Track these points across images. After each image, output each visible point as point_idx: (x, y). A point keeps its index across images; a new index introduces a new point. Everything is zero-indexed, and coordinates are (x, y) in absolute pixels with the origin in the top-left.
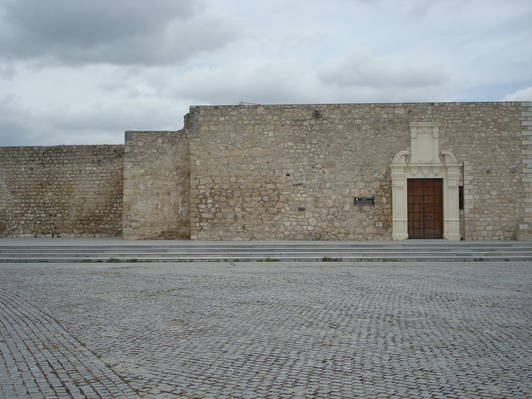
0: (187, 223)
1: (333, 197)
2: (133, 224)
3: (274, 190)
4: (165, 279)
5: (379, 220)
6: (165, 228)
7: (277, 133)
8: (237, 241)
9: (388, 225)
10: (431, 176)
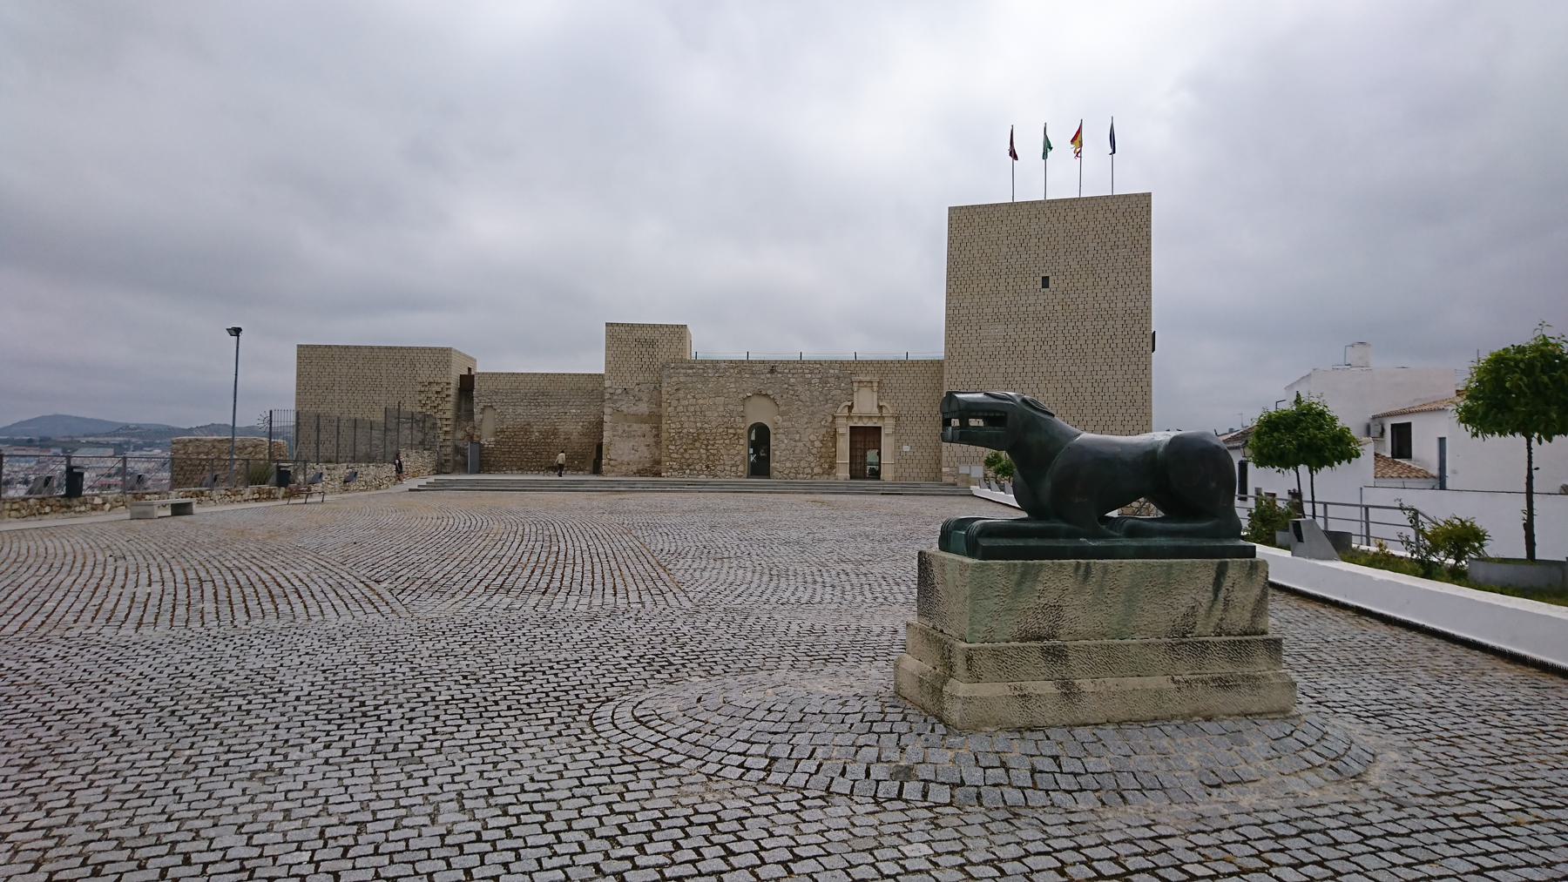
0: (658, 462)
8: (702, 478)
9: (832, 466)
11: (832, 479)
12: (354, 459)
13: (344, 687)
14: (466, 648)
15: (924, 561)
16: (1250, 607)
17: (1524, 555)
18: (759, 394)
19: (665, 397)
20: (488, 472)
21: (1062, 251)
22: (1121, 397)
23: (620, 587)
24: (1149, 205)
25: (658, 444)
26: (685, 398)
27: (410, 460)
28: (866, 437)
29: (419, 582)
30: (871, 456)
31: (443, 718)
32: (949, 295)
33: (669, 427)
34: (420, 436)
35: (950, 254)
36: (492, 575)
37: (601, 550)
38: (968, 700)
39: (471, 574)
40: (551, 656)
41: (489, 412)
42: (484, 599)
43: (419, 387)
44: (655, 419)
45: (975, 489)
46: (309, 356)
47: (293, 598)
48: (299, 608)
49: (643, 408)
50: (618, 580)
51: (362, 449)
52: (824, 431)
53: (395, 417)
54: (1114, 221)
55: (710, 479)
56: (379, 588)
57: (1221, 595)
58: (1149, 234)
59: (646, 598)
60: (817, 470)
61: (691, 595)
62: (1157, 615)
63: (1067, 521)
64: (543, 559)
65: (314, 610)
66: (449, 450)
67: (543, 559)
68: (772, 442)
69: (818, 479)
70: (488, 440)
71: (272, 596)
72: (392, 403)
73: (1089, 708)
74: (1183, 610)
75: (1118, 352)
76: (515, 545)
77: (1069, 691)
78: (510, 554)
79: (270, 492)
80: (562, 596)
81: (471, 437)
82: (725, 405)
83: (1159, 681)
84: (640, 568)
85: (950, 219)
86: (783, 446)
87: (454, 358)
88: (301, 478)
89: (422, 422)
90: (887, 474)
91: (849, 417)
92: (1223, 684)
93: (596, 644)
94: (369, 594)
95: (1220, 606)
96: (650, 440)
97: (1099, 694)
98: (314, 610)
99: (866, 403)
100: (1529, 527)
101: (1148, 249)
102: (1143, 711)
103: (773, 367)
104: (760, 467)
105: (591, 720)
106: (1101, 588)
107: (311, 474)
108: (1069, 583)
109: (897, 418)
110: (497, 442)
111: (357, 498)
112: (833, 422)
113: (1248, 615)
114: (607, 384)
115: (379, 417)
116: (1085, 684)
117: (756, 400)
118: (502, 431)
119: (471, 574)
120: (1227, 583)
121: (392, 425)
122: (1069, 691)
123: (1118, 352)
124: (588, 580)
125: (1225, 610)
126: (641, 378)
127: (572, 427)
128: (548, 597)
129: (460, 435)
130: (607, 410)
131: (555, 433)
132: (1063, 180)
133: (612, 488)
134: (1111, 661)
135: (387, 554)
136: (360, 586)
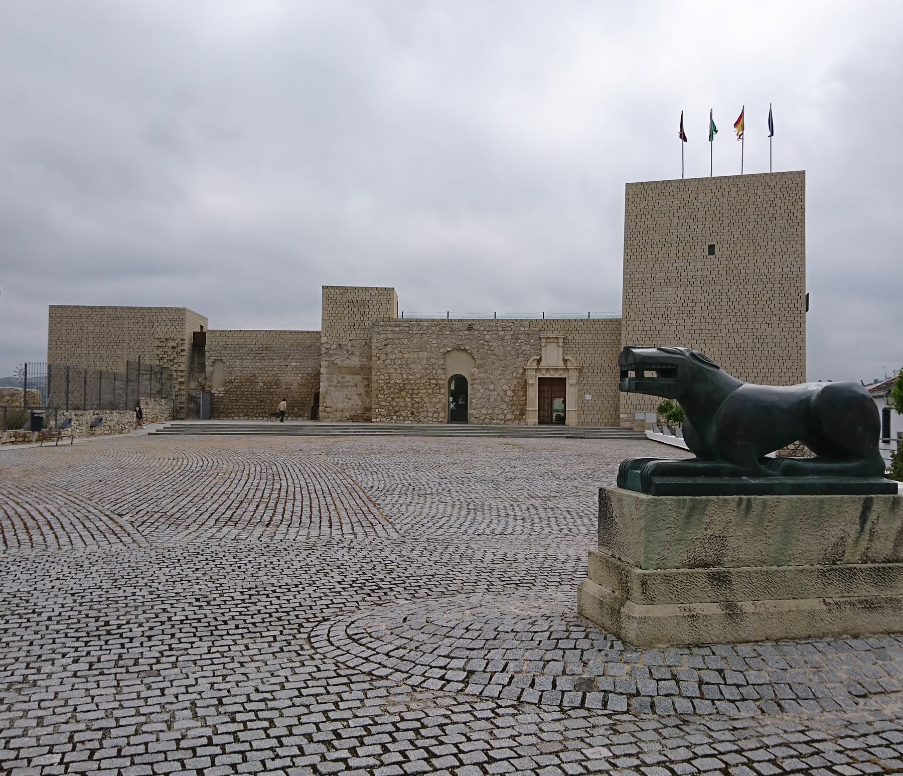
0: (369, 409)
1: (482, 391)
2: (328, 410)
3: (436, 385)
4: (568, 511)
5: (517, 409)
6: (353, 413)
7: (439, 341)
8: (408, 423)
9: (523, 413)
10: (556, 376)
11: (522, 424)
12: (100, 407)
14: (199, 574)
15: (604, 497)
18: (458, 349)
19: (374, 351)
20: (218, 418)
21: (726, 222)
22: (779, 351)
23: (335, 520)
24: (803, 182)
25: (368, 393)
26: (393, 352)
27: (149, 407)
28: (552, 387)
29: (157, 516)
30: (557, 403)
31: (178, 635)
33: (379, 379)
34: (158, 386)
36: (221, 510)
38: (643, 620)
39: (203, 509)
40: (273, 581)
41: (219, 365)
42: (214, 530)
43: (157, 343)
44: (366, 371)
45: (649, 433)
46: (58, 314)
47: (46, 529)
48: (51, 538)
49: (355, 361)
51: (107, 397)
52: (515, 382)
53: (136, 370)
54: (772, 196)
55: (415, 424)
56: (122, 521)
59: (358, 529)
60: (509, 416)
61: (398, 527)
62: (811, 545)
63: (730, 461)
64: (266, 495)
65: (64, 540)
66: (183, 398)
67: (266, 495)
69: (510, 424)
70: (218, 389)
71: (26, 528)
72: (133, 357)
73: (750, 628)
74: (833, 540)
75: (776, 311)
76: (242, 483)
77: (732, 612)
79: (25, 436)
80: (283, 528)
81: (203, 387)
83: (811, 603)
84: (352, 503)
85: (627, 194)
86: (479, 395)
87: (188, 317)
88: (52, 423)
89: (160, 373)
93: (314, 570)
94: (113, 526)
95: (866, 536)
96: (362, 390)
97: (759, 614)
98: (64, 540)
99: (552, 358)
101: (803, 220)
102: (798, 629)
103: (470, 325)
105: (309, 637)
107: (61, 419)
108: (732, 516)
109: (580, 370)
110: (226, 392)
111: (103, 441)
112: (523, 374)
113: (890, 545)
115: (122, 369)
116: (747, 606)
117: (455, 354)
118: (231, 382)
119: (203, 509)
121: (133, 377)
122: (732, 612)
123: (776, 311)
124: (306, 514)
125: (871, 540)
126: (353, 335)
127: (292, 378)
128: (271, 529)
129: (193, 385)
131: (277, 383)
132: (727, 160)
133: (327, 433)
134: (769, 585)
135: (128, 491)
136: (105, 519)
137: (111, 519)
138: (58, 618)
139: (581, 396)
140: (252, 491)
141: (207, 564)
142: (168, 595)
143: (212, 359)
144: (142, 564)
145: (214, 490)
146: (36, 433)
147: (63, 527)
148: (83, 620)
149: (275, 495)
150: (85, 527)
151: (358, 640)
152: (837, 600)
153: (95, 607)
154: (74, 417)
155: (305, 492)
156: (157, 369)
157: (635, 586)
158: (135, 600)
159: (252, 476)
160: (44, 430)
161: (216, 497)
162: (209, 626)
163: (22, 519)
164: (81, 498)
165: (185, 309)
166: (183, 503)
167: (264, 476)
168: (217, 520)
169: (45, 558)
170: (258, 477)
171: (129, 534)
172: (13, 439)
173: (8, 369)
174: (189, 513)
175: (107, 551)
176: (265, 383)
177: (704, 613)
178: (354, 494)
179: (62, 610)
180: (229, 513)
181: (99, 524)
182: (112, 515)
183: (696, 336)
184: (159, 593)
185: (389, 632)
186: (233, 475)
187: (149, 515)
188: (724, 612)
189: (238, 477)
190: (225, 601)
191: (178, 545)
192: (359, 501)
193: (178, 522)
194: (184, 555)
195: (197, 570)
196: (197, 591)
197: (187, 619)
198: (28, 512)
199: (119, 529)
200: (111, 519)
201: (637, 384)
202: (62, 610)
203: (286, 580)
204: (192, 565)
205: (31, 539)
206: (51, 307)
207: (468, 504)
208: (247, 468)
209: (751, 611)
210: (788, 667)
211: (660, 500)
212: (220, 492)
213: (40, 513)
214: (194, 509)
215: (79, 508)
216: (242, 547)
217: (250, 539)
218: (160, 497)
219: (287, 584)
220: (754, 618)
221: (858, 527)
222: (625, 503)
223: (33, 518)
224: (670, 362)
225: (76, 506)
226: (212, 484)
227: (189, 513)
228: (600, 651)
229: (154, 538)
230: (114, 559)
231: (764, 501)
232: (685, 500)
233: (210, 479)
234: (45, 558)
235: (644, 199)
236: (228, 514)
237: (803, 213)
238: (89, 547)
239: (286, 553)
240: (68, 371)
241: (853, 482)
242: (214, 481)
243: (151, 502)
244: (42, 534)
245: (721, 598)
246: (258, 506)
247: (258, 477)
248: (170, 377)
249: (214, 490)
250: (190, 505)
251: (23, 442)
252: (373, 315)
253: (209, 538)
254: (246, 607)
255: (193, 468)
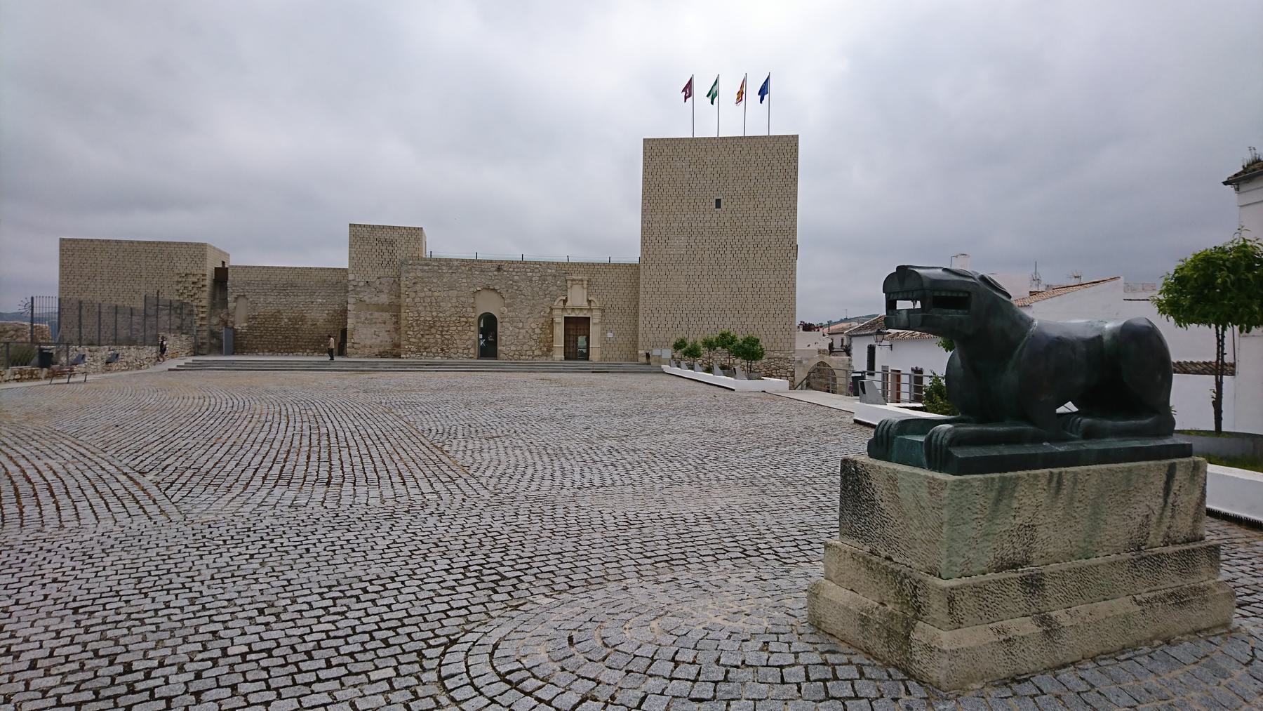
0: (398, 346)
6: (382, 349)
8: (438, 359)
9: (550, 349)
11: (550, 360)
12: (116, 342)
13: (103, 638)
14: (255, 564)
15: (849, 471)
16: (1192, 511)
17: (1213, 428)
18: (488, 289)
19: (403, 289)
20: (242, 353)
21: (731, 178)
22: (773, 295)
23: (406, 474)
24: (797, 145)
25: (397, 330)
26: (422, 291)
27: (172, 342)
28: (578, 326)
29: (188, 473)
30: (581, 340)
31: (243, 688)
32: (644, 211)
33: (407, 316)
34: (178, 321)
35: (644, 178)
36: (267, 463)
37: (370, 431)
38: (955, 654)
39: (245, 462)
40: (358, 571)
41: (242, 301)
42: (264, 493)
43: (176, 278)
44: (395, 309)
45: (666, 368)
46: (69, 248)
47: (44, 496)
48: (49, 510)
49: (384, 299)
50: (401, 465)
51: (123, 333)
52: (542, 320)
53: (154, 305)
54: (770, 156)
55: (445, 360)
56: (146, 481)
57: (1170, 501)
58: (796, 168)
59: (438, 486)
60: (537, 353)
61: (483, 481)
62: (1118, 527)
63: (1032, 423)
64: (315, 442)
65: (67, 513)
66: (205, 334)
67: (315, 442)
68: (499, 329)
69: (537, 360)
70: (241, 325)
71: (17, 495)
72: (152, 292)
73: (1070, 646)
74: (1139, 519)
75: (772, 260)
76: (283, 426)
77: (1050, 628)
78: (280, 436)
79: (32, 373)
80: (348, 485)
81: (225, 323)
82: (457, 297)
83: (1122, 605)
84: (417, 450)
85: (645, 148)
86: (508, 333)
87: (209, 252)
88: (64, 359)
89: (180, 309)
90: (595, 355)
91: (564, 309)
92: (1178, 599)
93: (406, 551)
94: (133, 489)
95: (1168, 513)
96: (390, 327)
97: (1077, 626)
98: (67, 513)
99: (577, 298)
100: (1217, 404)
101: (796, 180)
102: (1114, 642)
103: (499, 266)
104: (489, 350)
105: (441, 679)
106: (1072, 499)
107: (73, 356)
108: (1043, 497)
109: (603, 311)
110: (249, 328)
111: (118, 377)
112: (550, 313)
113: (1190, 521)
114: (351, 277)
115: (139, 305)
116: (1059, 614)
117: (485, 293)
118: (254, 318)
119: (245, 462)
120: (1175, 488)
121: (151, 312)
122: (1050, 628)
123: (772, 260)
124: (369, 468)
125: (1173, 517)
126: (381, 273)
127: (318, 314)
128: (333, 489)
129: (215, 321)
130: (351, 300)
131: (303, 319)
132: (729, 121)
133: (358, 369)
134: (1084, 584)
135: (150, 438)
136: (123, 478)
137: (131, 479)
138: (47, 663)
139: (603, 334)
140: (297, 438)
141: (264, 546)
142: (219, 604)
143: (235, 295)
144: (176, 549)
145: (253, 436)
146: (45, 370)
147: (67, 493)
148: (89, 664)
149: (324, 443)
150: (97, 491)
151: (518, 683)
152: (1147, 595)
153: (109, 634)
154: (87, 353)
155: (357, 437)
156: (175, 305)
157: (937, 606)
158: (169, 616)
159: (292, 419)
160: (54, 367)
161: (256, 447)
162: (287, 664)
163: (13, 482)
164: (93, 449)
165: (205, 245)
166: (219, 455)
167: (305, 419)
168: (264, 478)
169: (39, 544)
170: (298, 419)
171: (154, 501)
172: (18, 376)
173: (13, 304)
174: (228, 468)
175: (126, 529)
176: (290, 319)
177: (1021, 634)
178: (413, 439)
179: (55, 643)
180: (277, 468)
181: (115, 486)
182: (131, 473)
183: (705, 281)
184: (204, 600)
185: (557, 666)
186: (270, 417)
187: (179, 472)
188: (1041, 630)
189: (277, 420)
190: (300, 611)
191: (220, 517)
192: (422, 447)
193: (217, 481)
194: (231, 533)
195: (252, 556)
196: (258, 594)
197: (251, 652)
198: (23, 471)
199: (141, 493)
200: (131, 479)
201: (924, 318)
202: (55, 643)
203: (375, 570)
204: (243, 550)
205: (21, 513)
206: (62, 240)
207: (545, 448)
208: (283, 408)
209: (1068, 624)
210: (1135, 703)
211: (966, 481)
212: (260, 440)
213: (39, 472)
214: (233, 463)
215: (90, 464)
216: (305, 518)
217: (311, 504)
218: (189, 446)
219: (379, 578)
220: (1071, 632)
221: (1161, 500)
222: (900, 483)
223: (29, 480)
224: (963, 288)
225: (86, 461)
226: (249, 429)
227: (228, 468)
228: (895, 700)
229: (188, 507)
230: (135, 542)
231: (1075, 474)
232: (993, 479)
233: (246, 422)
234: (39, 544)
235: (659, 153)
236: (276, 469)
237: (796, 173)
238: (102, 522)
239: (362, 524)
240: (80, 309)
241: (1152, 444)
242: (251, 426)
243: (179, 454)
244: (39, 505)
245: (1033, 609)
246: (309, 458)
247: (298, 419)
248: (191, 313)
249: (253, 436)
250: (227, 457)
251: (30, 379)
252: (401, 254)
253: (260, 505)
254: (333, 622)
255: (223, 409)
